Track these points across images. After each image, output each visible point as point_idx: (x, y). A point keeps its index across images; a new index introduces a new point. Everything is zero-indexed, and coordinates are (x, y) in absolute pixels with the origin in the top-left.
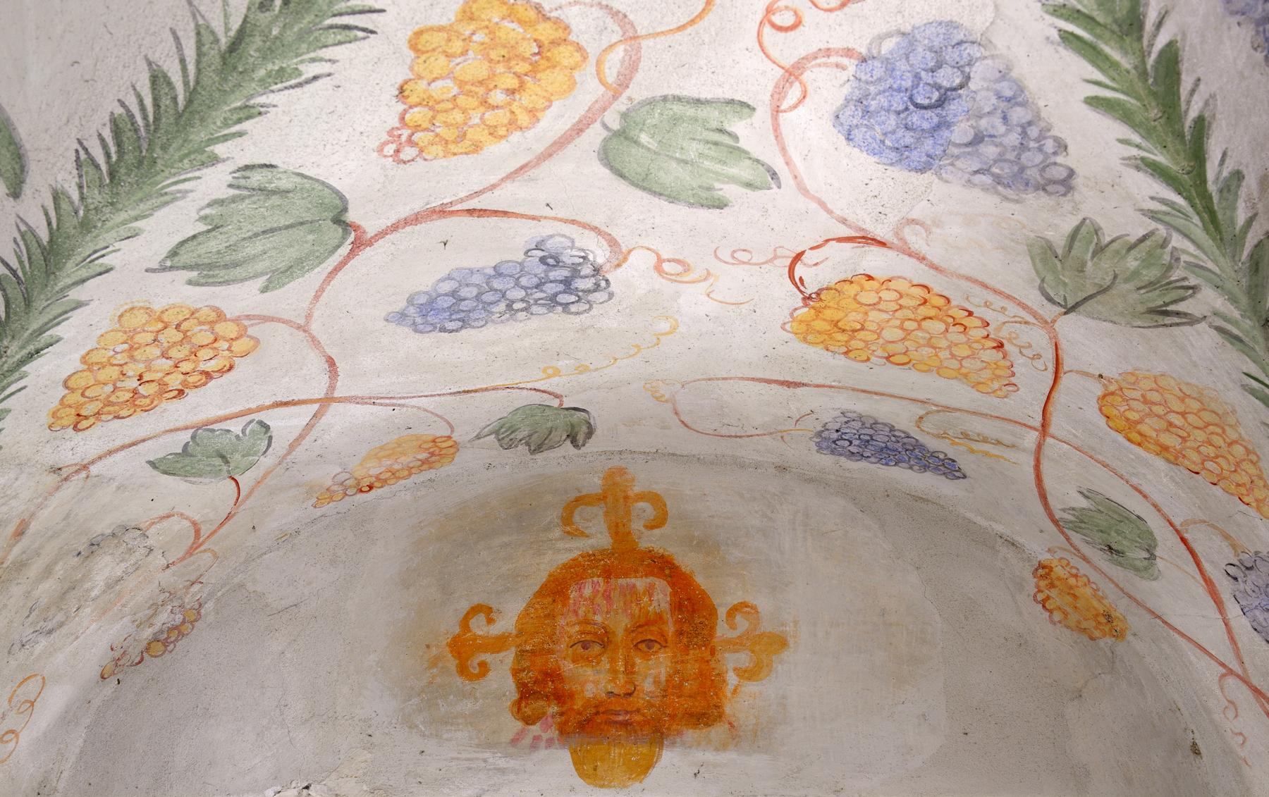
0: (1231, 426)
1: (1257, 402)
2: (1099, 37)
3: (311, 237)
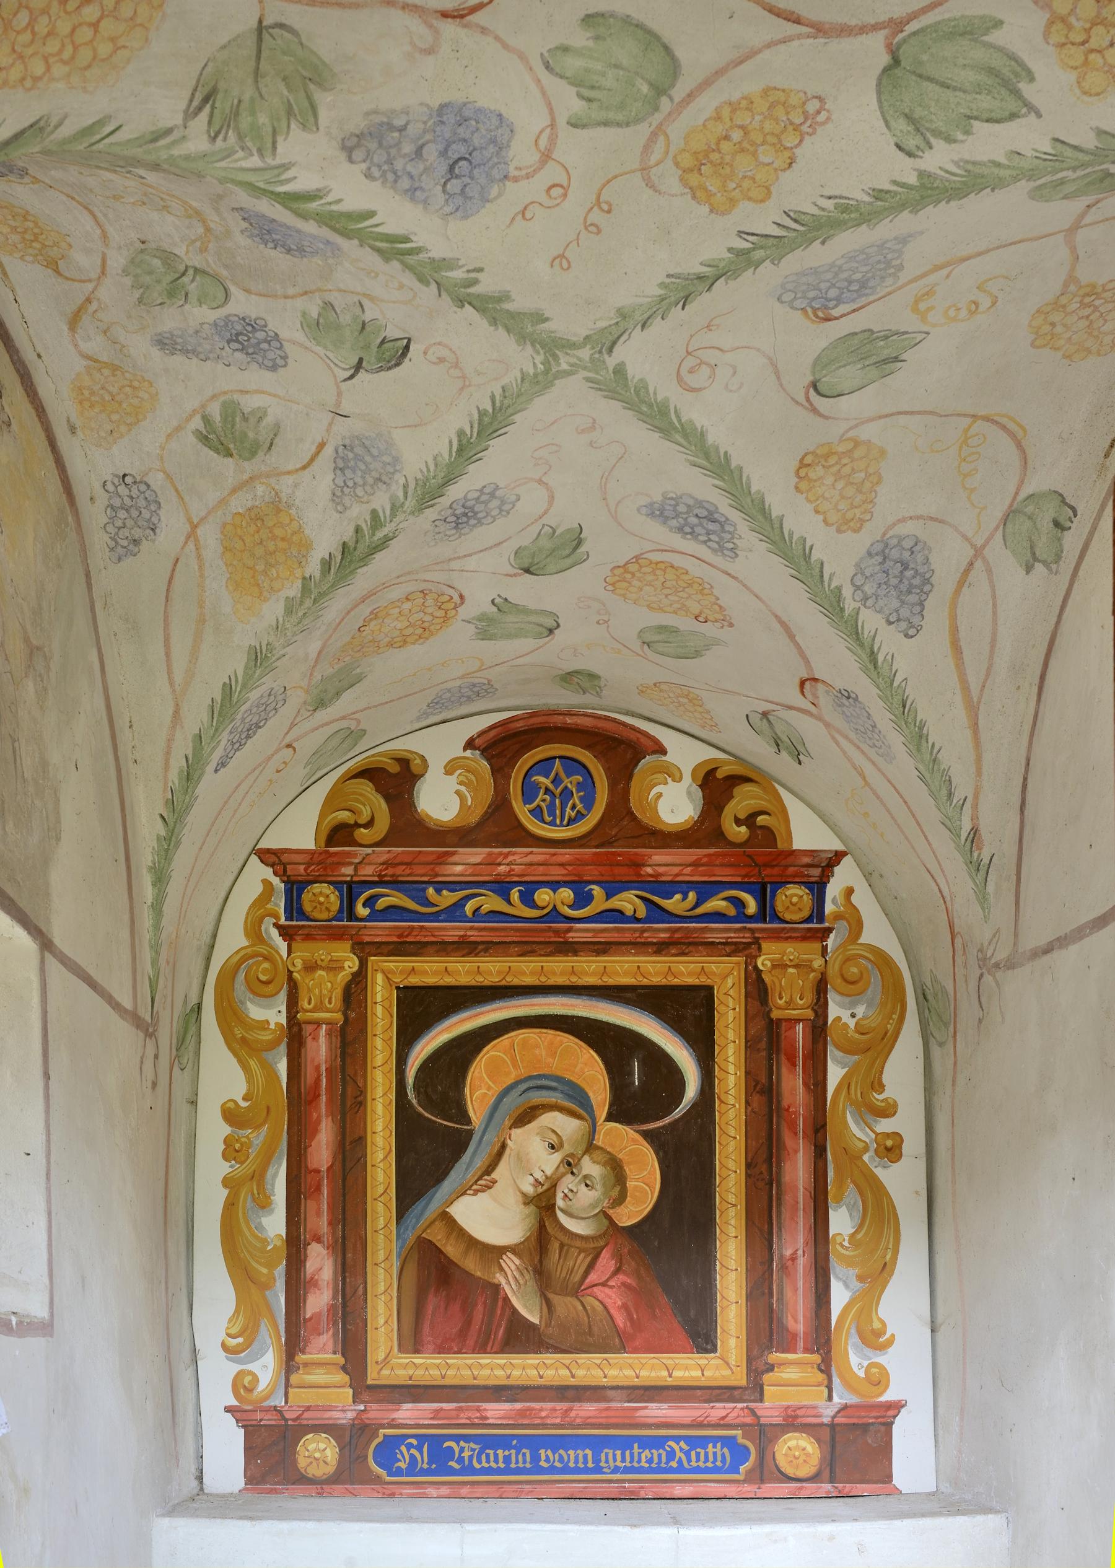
0: (69, 75)
1: (90, 122)
2: (393, 248)
3: (925, 57)
